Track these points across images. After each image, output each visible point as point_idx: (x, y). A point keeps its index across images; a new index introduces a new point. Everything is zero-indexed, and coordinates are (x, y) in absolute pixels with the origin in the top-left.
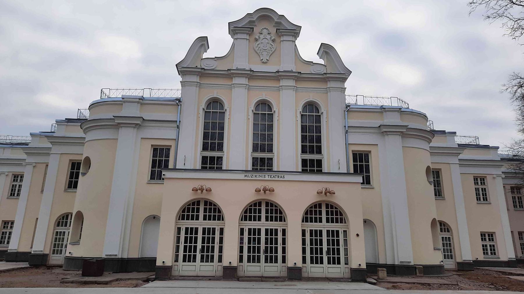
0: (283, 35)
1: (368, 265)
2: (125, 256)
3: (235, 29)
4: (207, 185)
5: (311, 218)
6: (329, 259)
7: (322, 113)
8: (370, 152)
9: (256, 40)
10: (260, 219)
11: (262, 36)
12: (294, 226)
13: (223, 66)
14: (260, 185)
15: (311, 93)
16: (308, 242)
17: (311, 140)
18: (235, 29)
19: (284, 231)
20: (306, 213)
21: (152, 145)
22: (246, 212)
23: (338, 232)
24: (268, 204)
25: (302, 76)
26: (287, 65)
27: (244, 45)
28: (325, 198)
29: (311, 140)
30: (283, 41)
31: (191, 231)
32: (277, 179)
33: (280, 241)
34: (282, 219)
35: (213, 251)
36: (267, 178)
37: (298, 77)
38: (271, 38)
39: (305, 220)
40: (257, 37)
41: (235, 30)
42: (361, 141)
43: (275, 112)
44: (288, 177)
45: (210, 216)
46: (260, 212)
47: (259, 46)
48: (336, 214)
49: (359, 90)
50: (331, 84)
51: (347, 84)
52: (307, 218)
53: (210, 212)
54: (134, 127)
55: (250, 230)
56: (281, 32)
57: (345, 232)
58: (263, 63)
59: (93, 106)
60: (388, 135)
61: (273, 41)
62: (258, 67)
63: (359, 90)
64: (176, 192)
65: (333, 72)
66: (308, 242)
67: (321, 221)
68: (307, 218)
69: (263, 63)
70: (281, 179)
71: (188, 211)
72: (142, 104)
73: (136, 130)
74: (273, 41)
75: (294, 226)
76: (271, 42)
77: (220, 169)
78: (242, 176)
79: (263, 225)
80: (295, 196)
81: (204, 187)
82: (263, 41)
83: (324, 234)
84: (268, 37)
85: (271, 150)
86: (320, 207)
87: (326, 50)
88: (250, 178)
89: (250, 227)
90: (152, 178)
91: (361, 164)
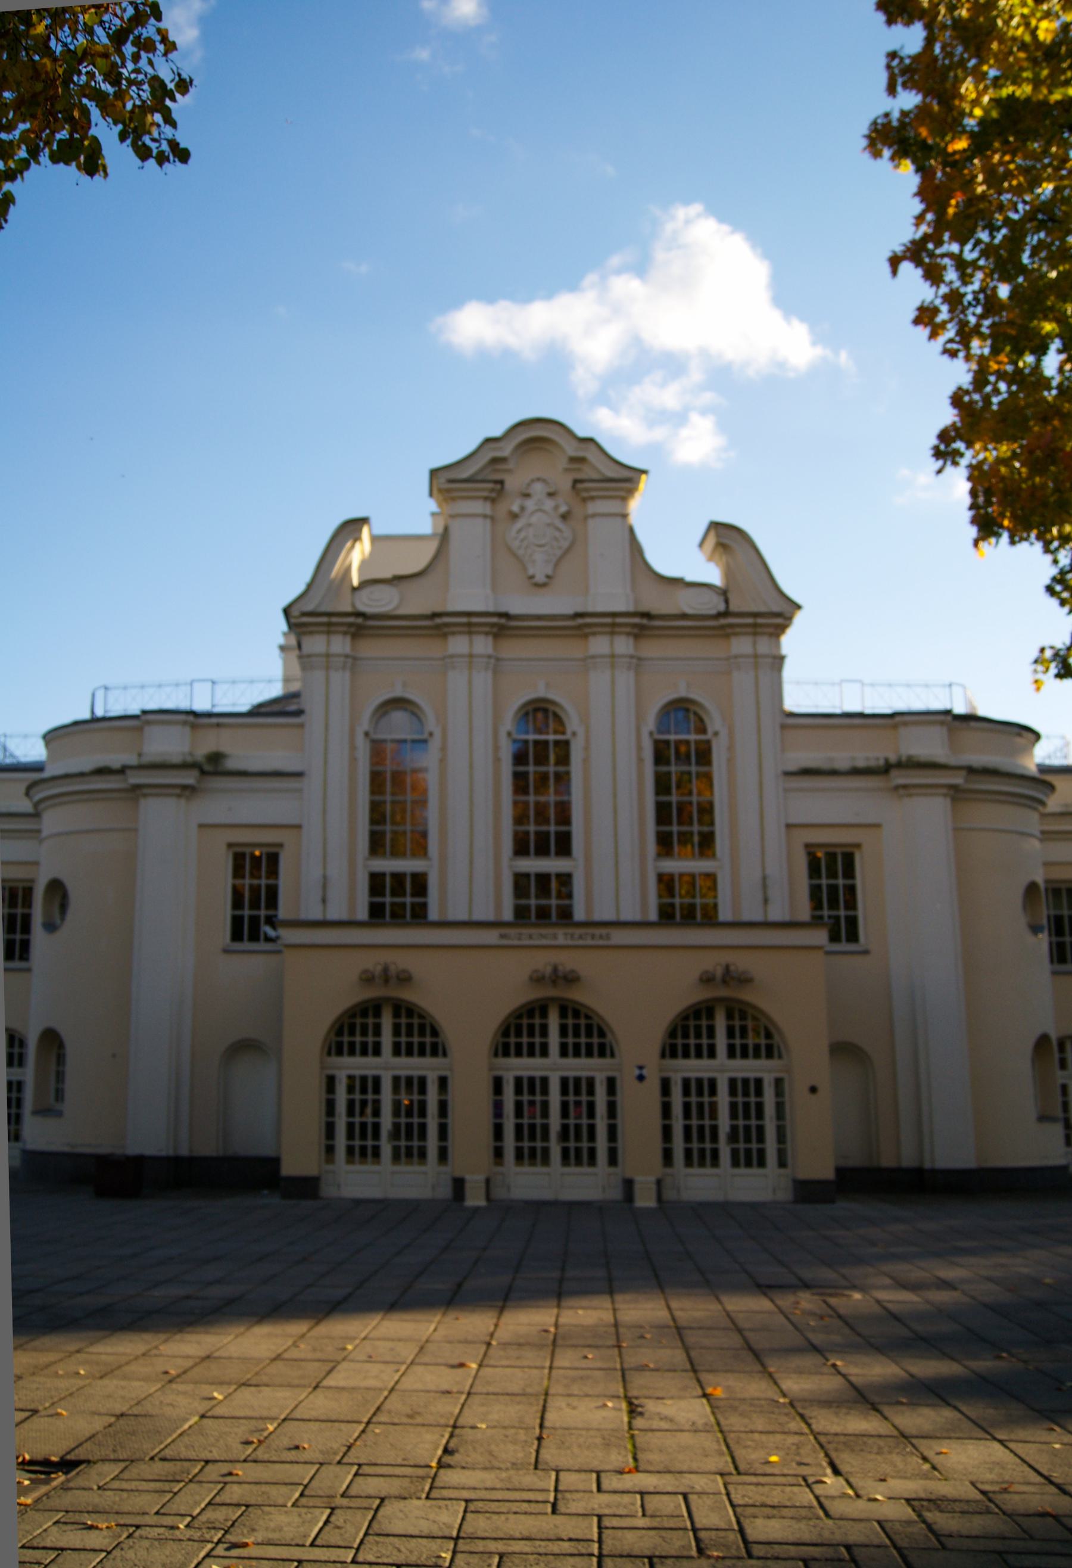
0: (592, 498)
1: (839, 1171)
2: (184, 1152)
3: (446, 482)
4: (401, 961)
5: (686, 1047)
6: (735, 1153)
7: (716, 734)
8: (858, 846)
9: (514, 516)
10: (544, 1052)
11: (530, 504)
12: (469, 1068)
13: (418, 602)
14: (542, 961)
15: (679, 670)
16: (677, 1109)
17: (682, 811)
18: (446, 482)
19: (443, 1082)
20: (672, 1034)
21: (230, 845)
22: (506, 1033)
23: (759, 1082)
24: (566, 1009)
25: (655, 618)
26: (611, 595)
27: (473, 535)
28: (723, 992)
29: (682, 811)
30: (594, 516)
31: (367, 1086)
32: (590, 942)
33: (601, 1108)
34: (437, 1050)
35: (423, 1135)
36: (561, 940)
37: (643, 624)
38: (556, 508)
39: (503, 1049)
40: (515, 508)
41: (448, 491)
42: (832, 810)
43: (574, 734)
44: (620, 937)
45: (577, 1046)
46: (544, 1032)
47: (522, 535)
48: (754, 1035)
49: (824, 671)
50: (741, 645)
51: (789, 642)
52: (506, 1046)
53: (409, 1034)
54: (179, 796)
55: (518, 1081)
56: (587, 490)
57: (443, 1082)
58: (538, 585)
59: (51, 737)
60: (910, 795)
61: (564, 517)
62: (519, 604)
63: (824, 671)
64: (320, 984)
65: (750, 613)
66: (677, 1109)
67: (377, 1052)
68: (506, 1046)
69: (538, 585)
70: (601, 942)
71: (351, 1032)
72: (194, 727)
73: (183, 801)
74: (564, 517)
75: (469, 1068)
76: (558, 522)
77: (419, 915)
78: (490, 937)
79: (554, 1067)
80: (639, 990)
81: (392, 968)
82: (534, 519)
83: (723, 1088)
84: (549, 504)
85: (564, 847)
86: (544, 1014)
87: (726, 538)
88: (516, 942)
89: (519, 1073)
90: (237, 936)
91: (833, 881)
